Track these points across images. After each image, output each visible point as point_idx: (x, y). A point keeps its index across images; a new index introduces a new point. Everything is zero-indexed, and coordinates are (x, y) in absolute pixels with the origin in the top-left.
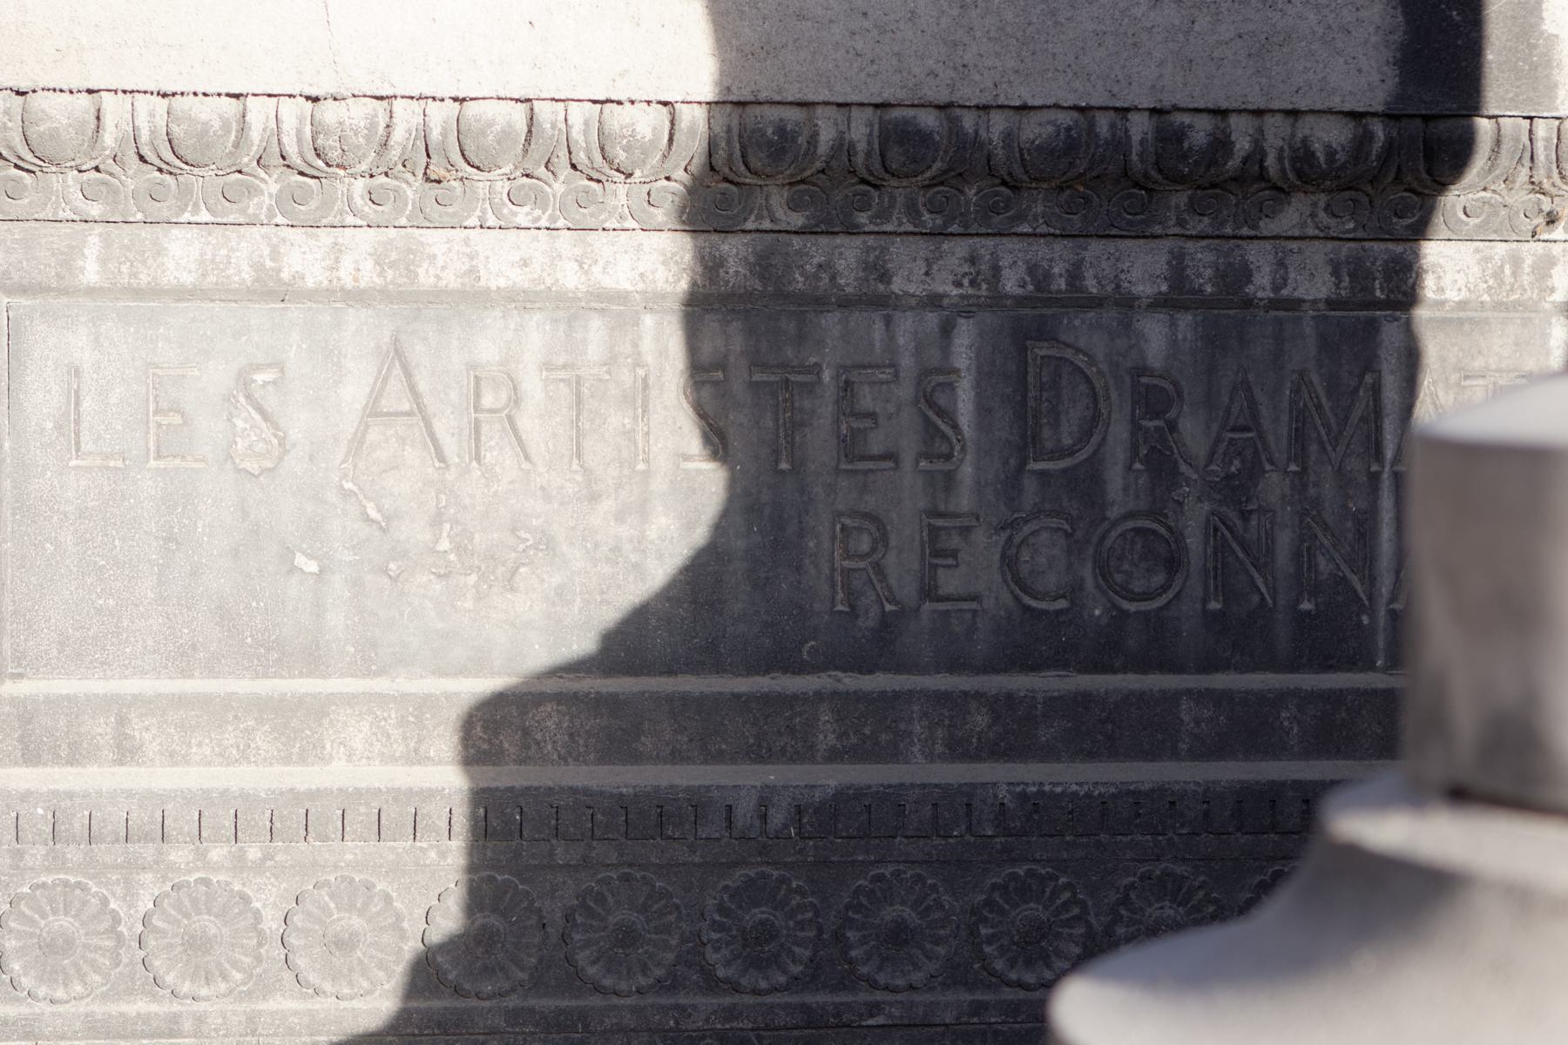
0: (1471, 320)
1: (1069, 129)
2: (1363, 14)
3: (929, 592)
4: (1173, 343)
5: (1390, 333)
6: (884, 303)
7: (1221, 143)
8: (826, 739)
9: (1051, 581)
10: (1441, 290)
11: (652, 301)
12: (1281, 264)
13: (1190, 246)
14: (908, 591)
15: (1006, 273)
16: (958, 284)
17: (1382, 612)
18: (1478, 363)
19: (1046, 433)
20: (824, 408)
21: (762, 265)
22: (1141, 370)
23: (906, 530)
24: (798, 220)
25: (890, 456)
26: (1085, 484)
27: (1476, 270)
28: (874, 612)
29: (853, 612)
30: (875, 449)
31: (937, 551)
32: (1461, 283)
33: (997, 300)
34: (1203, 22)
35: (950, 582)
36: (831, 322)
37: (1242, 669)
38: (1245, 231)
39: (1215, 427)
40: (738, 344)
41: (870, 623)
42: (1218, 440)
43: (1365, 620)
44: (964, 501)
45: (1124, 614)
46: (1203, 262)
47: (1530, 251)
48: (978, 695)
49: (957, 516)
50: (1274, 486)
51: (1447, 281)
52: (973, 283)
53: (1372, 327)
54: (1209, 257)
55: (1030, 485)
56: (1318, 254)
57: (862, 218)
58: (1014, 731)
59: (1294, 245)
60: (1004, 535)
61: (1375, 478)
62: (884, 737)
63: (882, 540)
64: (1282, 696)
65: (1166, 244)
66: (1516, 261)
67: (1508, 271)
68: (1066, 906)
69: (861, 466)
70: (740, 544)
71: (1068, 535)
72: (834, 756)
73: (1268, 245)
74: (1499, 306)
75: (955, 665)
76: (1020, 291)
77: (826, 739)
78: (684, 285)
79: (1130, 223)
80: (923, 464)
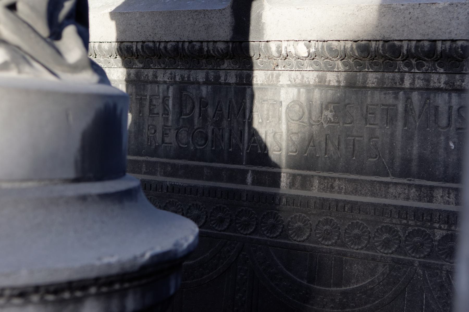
0: (265, 88)
1: (174, 46)
2: (227, 19)
3: (163, 142)
4: (207, 92)
5: (248, 91)
6: (157, 82)
7: (201, 49)
8: (144, 170)
9: (184, 141)
10: (257, 81)
11: (120, 81)
12: (226, 75)
13: (210, 71)
14: (160, 141)
15: (177, 77)
16: (169, 79)
17: (245, 152)
18: (266, 98)
19: (184, 110)
20: (147, 103)
21: (137, 75)
22: (201, 98)
23: (159, 129)
24: (141, 66)
25: (158, 114)
26: (191, 121)
27: (264, 77)
28: (154, 145)
29: (151, 145)
30: (155, 112)
31: (164, 134)
32: (261, 80)
33: (175, 82)
34: (197, 22)
35: (167, 140)
36: (149, 86)
37: (218, 162)
38: (218, 68)
39: (214, 110)
40: (134, 90)
41: (153, 147)
42: (215, 113)
43: (242, 154)
44: (170, 124)
45: (196, 149)
46: (212, 74)
47: (275, 73)
48: (169, 163)
49: (169, 126)
50: (225, 123)
51: (258, 79)
52: (171, 79)
53: (245, 89)
54: (213, 74)
55: (181, 120)
56: (233, 73)
57: (151, 65)
58: (175, 171)
59: (229, 71)
60: (176, 131)
61: (244, 122)
62: (153, 170)
63: (155, 131)
64: (223, 169)
65: (205, 71)
66: (272, 75)
67: (271, 77)
68: (179, 208)
69: (154, 115)
70: (133, 130)
71: (187, 132)
72: (145, 173)
73: (224, 71)
74: (269, 85)
75: (167, 157)
76: (179, 80)
77: (144, 170)
78: (124, 79)
79: (197, 66)
80: (164, 116)
